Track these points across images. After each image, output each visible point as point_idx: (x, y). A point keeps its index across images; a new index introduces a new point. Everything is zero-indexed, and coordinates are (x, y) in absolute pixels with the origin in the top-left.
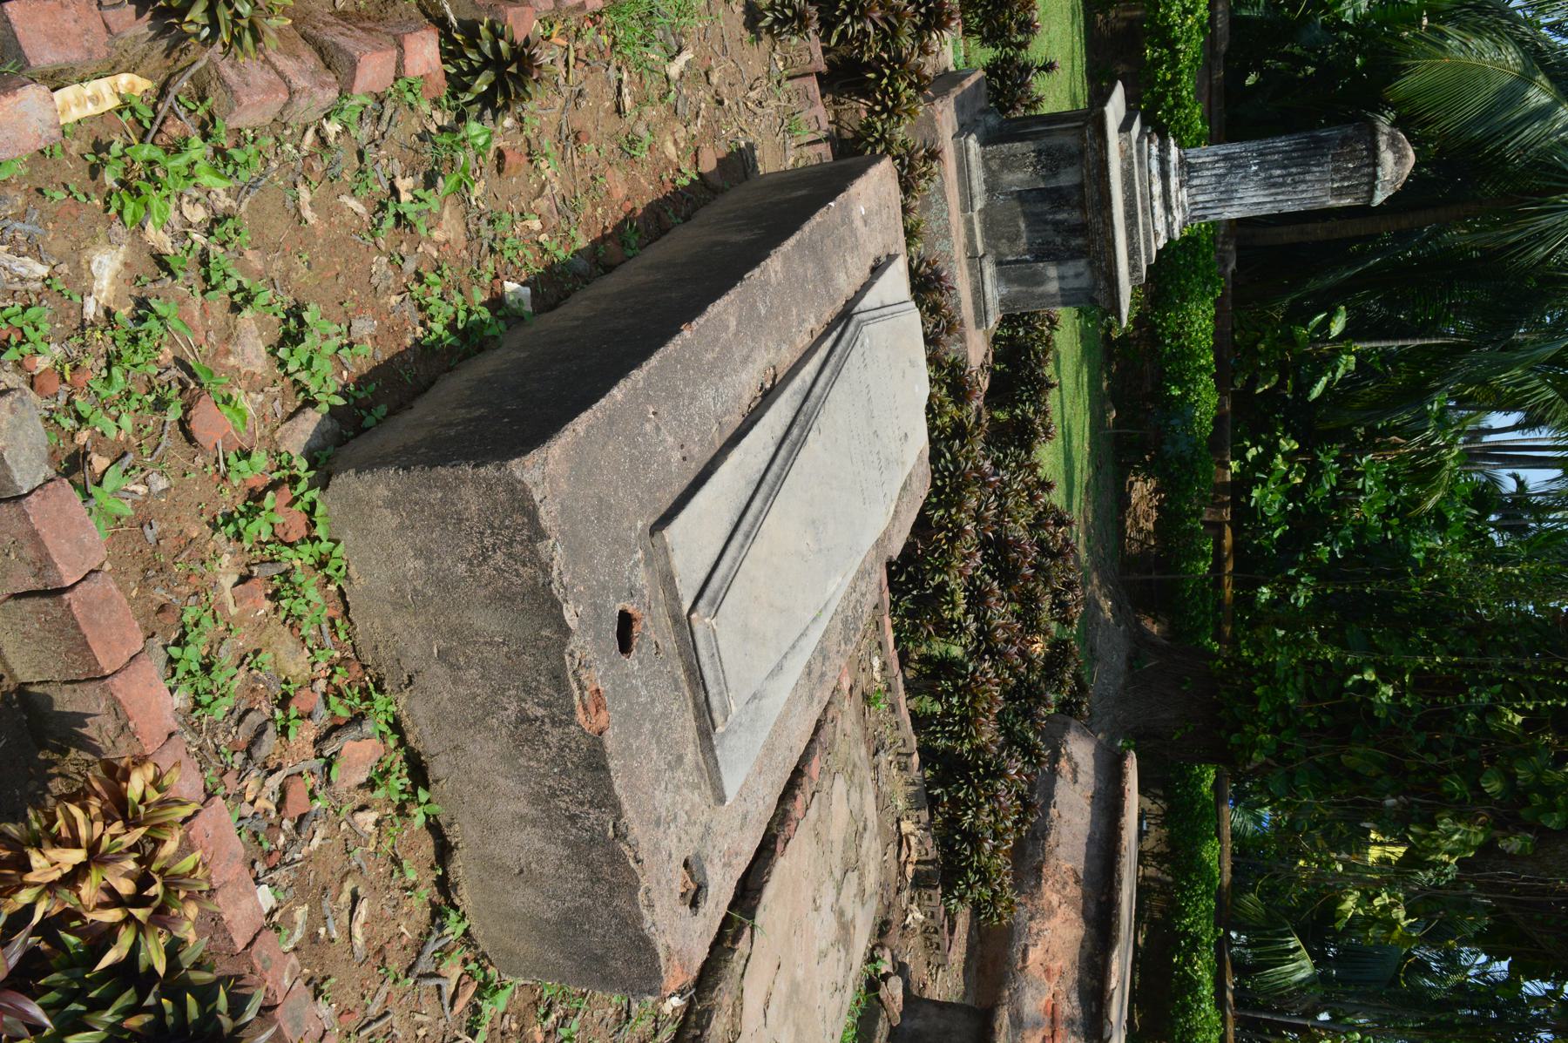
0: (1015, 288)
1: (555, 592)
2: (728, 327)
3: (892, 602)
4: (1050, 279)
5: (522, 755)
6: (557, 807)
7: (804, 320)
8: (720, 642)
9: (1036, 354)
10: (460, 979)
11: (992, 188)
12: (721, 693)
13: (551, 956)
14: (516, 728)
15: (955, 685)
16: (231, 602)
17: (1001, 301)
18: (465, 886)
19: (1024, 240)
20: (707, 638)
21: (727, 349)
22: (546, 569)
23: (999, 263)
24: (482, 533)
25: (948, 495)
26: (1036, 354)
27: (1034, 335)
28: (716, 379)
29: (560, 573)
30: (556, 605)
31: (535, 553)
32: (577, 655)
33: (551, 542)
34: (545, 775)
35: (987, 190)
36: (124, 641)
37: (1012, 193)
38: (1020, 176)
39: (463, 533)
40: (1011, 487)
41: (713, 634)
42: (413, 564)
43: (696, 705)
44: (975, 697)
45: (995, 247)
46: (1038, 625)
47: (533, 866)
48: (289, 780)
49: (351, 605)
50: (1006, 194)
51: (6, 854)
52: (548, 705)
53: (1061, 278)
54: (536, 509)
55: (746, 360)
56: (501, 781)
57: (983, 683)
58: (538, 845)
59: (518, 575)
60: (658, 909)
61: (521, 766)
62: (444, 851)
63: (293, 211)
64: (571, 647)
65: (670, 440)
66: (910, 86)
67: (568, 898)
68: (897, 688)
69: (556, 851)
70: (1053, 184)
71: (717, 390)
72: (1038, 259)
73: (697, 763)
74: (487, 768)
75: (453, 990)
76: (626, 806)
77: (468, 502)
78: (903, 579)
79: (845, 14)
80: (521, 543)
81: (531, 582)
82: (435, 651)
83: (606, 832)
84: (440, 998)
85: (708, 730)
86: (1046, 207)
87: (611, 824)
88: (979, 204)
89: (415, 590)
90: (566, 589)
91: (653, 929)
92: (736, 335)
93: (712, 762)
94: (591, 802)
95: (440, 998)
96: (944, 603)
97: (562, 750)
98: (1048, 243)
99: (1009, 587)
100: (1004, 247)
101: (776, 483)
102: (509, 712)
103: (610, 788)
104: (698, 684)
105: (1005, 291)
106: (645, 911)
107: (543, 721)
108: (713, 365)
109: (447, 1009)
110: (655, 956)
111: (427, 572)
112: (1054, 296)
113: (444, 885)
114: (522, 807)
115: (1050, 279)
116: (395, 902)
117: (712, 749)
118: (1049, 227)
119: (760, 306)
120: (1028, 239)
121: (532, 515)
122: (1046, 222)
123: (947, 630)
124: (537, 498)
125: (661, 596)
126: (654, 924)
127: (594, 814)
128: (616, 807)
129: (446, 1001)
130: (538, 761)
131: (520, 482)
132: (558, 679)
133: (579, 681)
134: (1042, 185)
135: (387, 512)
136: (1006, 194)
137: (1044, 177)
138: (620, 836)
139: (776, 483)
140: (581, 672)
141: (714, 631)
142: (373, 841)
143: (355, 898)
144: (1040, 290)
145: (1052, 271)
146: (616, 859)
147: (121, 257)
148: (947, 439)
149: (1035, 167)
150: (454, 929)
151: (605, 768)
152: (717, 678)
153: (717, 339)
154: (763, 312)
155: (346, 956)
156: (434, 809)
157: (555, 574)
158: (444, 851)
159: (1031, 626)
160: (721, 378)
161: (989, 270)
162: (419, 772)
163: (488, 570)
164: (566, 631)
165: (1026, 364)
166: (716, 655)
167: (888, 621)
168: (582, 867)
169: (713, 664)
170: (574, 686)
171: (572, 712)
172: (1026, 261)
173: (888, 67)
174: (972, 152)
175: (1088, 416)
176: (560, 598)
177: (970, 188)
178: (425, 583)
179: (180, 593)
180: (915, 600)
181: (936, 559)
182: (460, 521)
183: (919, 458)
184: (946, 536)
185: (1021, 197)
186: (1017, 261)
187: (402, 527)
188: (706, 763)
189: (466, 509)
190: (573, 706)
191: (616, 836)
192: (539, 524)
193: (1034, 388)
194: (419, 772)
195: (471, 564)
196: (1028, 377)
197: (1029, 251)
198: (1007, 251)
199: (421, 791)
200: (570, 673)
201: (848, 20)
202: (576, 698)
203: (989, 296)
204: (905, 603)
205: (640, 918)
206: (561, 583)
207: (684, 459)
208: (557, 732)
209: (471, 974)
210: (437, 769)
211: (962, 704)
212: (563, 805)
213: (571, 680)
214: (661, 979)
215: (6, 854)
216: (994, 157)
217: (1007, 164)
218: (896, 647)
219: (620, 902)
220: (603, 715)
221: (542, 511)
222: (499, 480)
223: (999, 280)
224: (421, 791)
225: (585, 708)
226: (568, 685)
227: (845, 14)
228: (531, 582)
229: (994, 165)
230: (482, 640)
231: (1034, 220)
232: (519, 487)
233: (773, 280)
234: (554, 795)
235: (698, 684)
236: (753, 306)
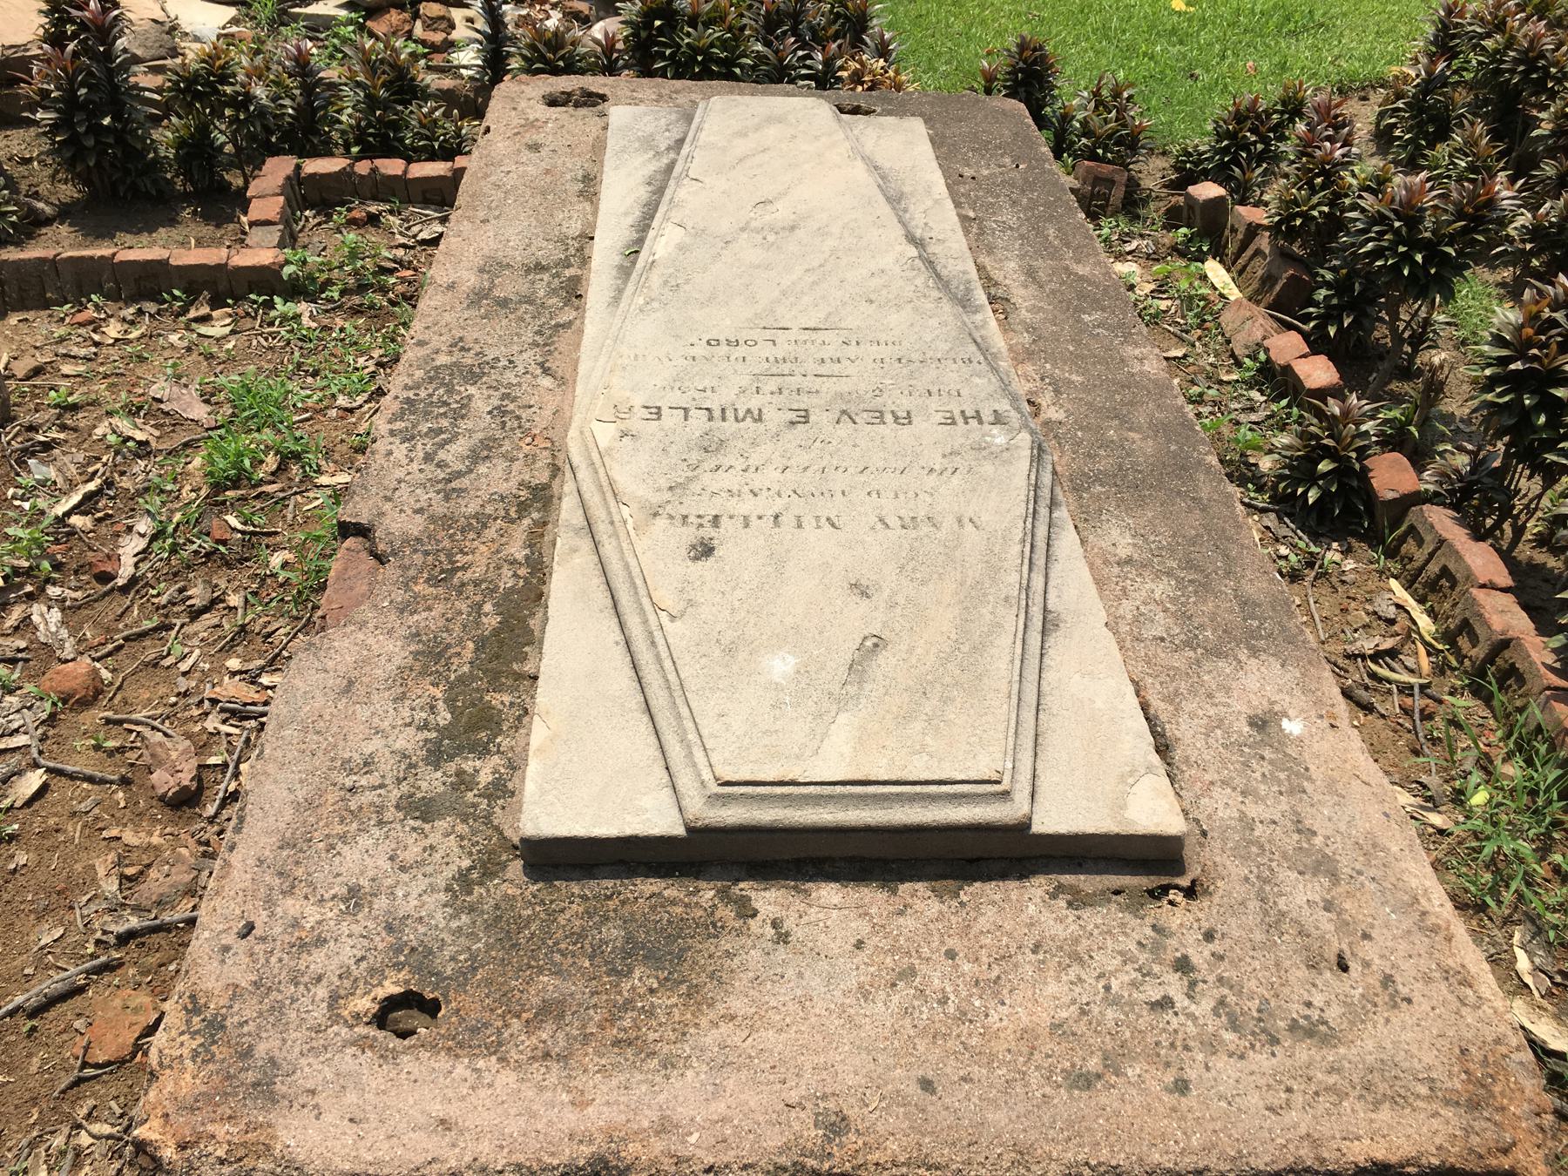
2: (1078, 262)
7: (1057, 392)
21: (1054, 254)
28: (1024, 230)
36: (726, 762)
48: (676, 134)
51: (1560, 393)
55: (1031, 273)
65: (986, 172)
71: (1011, 228)
92: (1067, 268)
108: (1040, 232)
119: (1097, 315)
153: (1068, 245)
154: (1086, 317)
160: (1022, 237)
179: (487, 670)
186: (1448, 324)
207: (961, 176)
215: (1560, 393)
233: (1130, 351)
236: (1097, 305)
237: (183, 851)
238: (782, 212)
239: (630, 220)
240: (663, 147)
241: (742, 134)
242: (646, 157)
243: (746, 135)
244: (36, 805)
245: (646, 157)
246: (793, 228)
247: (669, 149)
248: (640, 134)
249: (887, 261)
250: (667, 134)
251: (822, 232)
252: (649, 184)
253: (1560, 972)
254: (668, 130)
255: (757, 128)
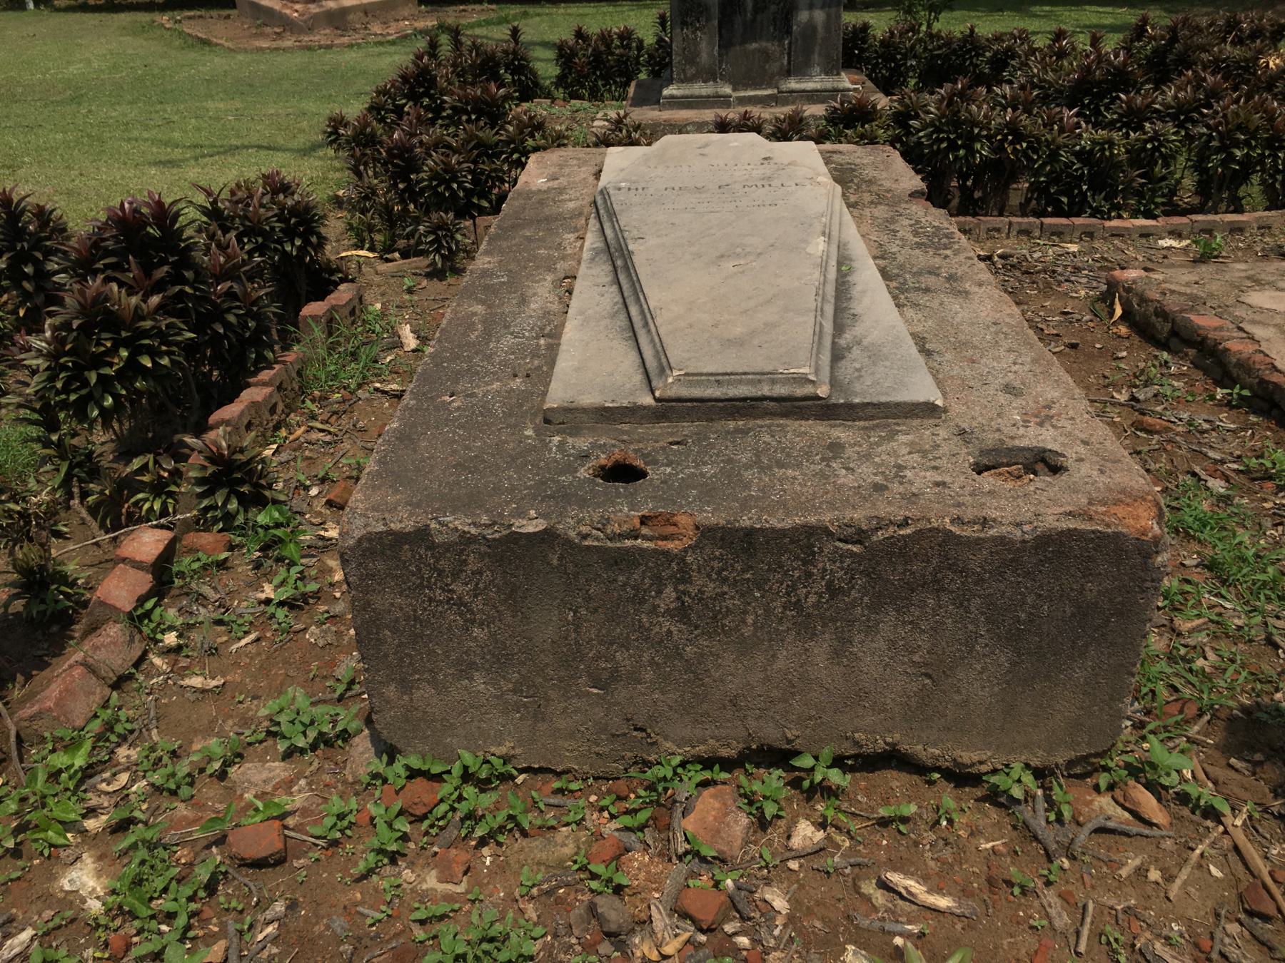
0: (816, 57)
1: (497, 536)
3: (1092, 216)
4: (811, 18)
5: (737, 629)
6: (817, 605)
8: (705, 371)
9: (940, 48)
10: (1117, 802)
11: (710, 75)
12: (773, 382)
13: (1078, 674)
14: (697, 627)
15: (1218, 150)
16: (450, 887)
17: (827, 74)
18: (959, 752)
19: (769, 45)
20: (691, 384)
22: (467, 540)
23: (788, 73)
24: (430, 600)
25: (959, 137)
26: (940, 48)
27: (919, 49)
29: (474, 524)
30: (515, 538)
31: (447, 547)
32: (585, 529)
33: (433, 525)
34: (768, 611)
35: (715, 81)
37: (720, 55)
38: (703, 45)
39: (433, 620)
40: (1034, 76)
41: (692, 377)
42: (479, 682)
43: (785, 415)
44: (1239, 128)
45: (773, 76)
46: (1246, 60)
47: (916, 658)
49: (544, 765)
50: (721, 62)
52: (659, 583)
53: (811, 7)
54: (390, 533)
56: (780, 664)
57: (1225, 116)
58: (882, 645)
59: (480, 573)
60: (994, 514)
61: (754, 634)
62: (895, 759)
63: (199, 696)
64: (572, 534)
66: (533, 136)
67: (971, 627)
68: (1209, 222)
69: (888, 623)
70: (715, 11)
72: (789, 32)
73: (859, 429)
74: (762, 676)
75: (1127, 815)
76: (812, 520)
77: (392, 604)
78: (1065, 200)
79: (449, 188)
80: (438, 560)
81: (487, 560)
82: (596, 691)
83: (852, 554)
84: (1127, 835)
85: (822, 406)
86: (738, 19)
87: (841, 545)
88: (727, 90)
89: (514, 691)
90: (494, 523)
91: (1026, 528)
93: (870, 411)
94: (805, 563)
95: (1127, 835)
96: (1103, 153)
97: (725, 580)
98: (774, 19)
99: (1136, 82)
100: (773, 67)
101: (635, 289)
102: (673, 628)
103: (782, 533)
104: (752, 407)
105: (818, 69)
106: (992, 532)
107: (684, 593)
109: (1155, 832)
110: (1070, 533)
111: (488, 671)
112: (829, 16)
113: (961, 777)
114: (820, 650)
115: (811, 18)
116: (941, 843)
117: (850, 407)
118: (759, 18)
120: (768, 40)
121: (399, 539)
122: (754, 20)
123: (1153, 155)
124: (381, 528)
125: (626, 427)
126: (1019, 525)
127: (823, 563)
128: (811, 532)
129: (1136, 828)
130: (745, 612)
131: (360, 541)
132: (621, 560)
133: (622, 536)
134: (716, 23)
135: (417, 694)
136: (721, 62)
137: (708, 20)
138: (859, 536)
139: (635, 289)
140: (609, 531)
141: (687, 374)
142: (839, 838)
143: (884, 886)
144: (820, 29)
145: (803, 16)
146: (899, 550)
147: (89, 861)
148: (908, 134)
149: (697, 29)
150: (1019, 783)
151: (750, 533)
152: (751, 382)
155: (959, 926)
156: (827, 753)
157: (473, 531)
158: (895, 759)
159: (1246, 69)
161: (793, 84)
162: (779, 757)
163: (478, 604)
164: (548, 537)
165: (946, 58)
166: (718, 378)
167: (1115, 223)
168: (915, 598)
169: (729, 383)
170: (628, 543)
171: (666, 553)
172: (790, 43)
173: (512, 154)
174: (675, 92)
175: (1087, 7)
176: (505, 533)
177: (708, 97)
178: (504, 677)
180: (1095, 189)
181: (1039, 157)
182: (416, 618)
183: (142, 30)
184: (1012, 143)
185: (725, 45)
186: (789, 55)
187: (433, 683)
188: (872, 418)
189: (401, 609)
190: (655, 551)
191: (859, 542)
192: (410, 533)
193: (969, 51)
194: (779, 757)
195: (473, 622)
196: (958, 57)
197: (781, 40)
198: (778, 64)
199: (797, 762)
200: (609, 544)
201: (455, 186)
202: (646, 544)
203: (818, 86)
204: (1098, 201)
205: (1002, 540)
206: (487, 526)
208: (699, 580)
209: (1111, 787)
210: (771, 734)
211: (1247, 143)
212: (812, 599)
213: (618, 545)
214: (1117, 535)
216: (684, 71)
217: (691, 59)
218: (1155, 217)
219: (975, 563)
220: (682, 519)
221: (395, 526)
222: (361, 564)
223: (804, 75)
224: (797, 762)
225: (665, 538)
226: (627, 550)
227: (449, 188)
228: (487, 560)
229: (691, 71)
230: (573, 635)
231: (751, 34)
232: (365, 545)
234: (798, 605)
235: (752, 407)
237: (657, 895)
238: (729, 265)
239: (858, 288)
240: (856, 351)
241: (770, 326)
242: (869, 339)
243: (766, 324)
244: (928, 914)
245: (869, 339)
246: (722, 256)
247: (849, 349)
248: (888, 363)
249: (652, 241)
250: (858, 366)
251: (698, 255)
252: (854, 315)
253: (6, 347)
254: (857, 370)
255: (753, 334)
